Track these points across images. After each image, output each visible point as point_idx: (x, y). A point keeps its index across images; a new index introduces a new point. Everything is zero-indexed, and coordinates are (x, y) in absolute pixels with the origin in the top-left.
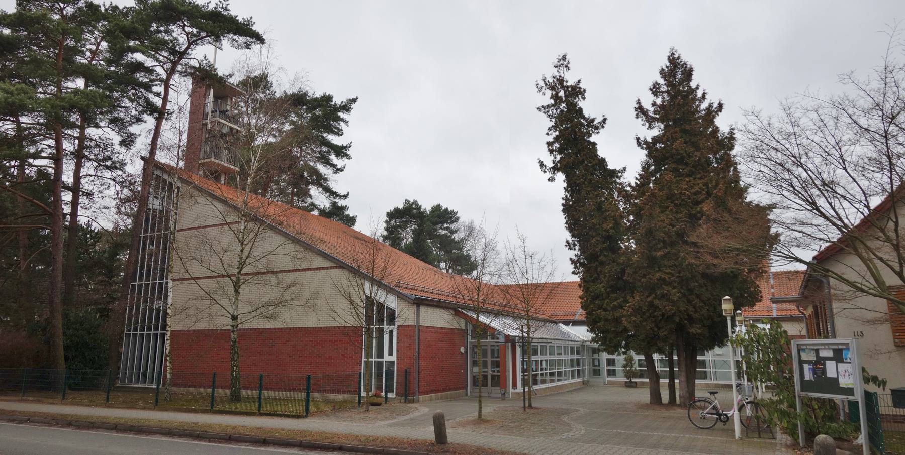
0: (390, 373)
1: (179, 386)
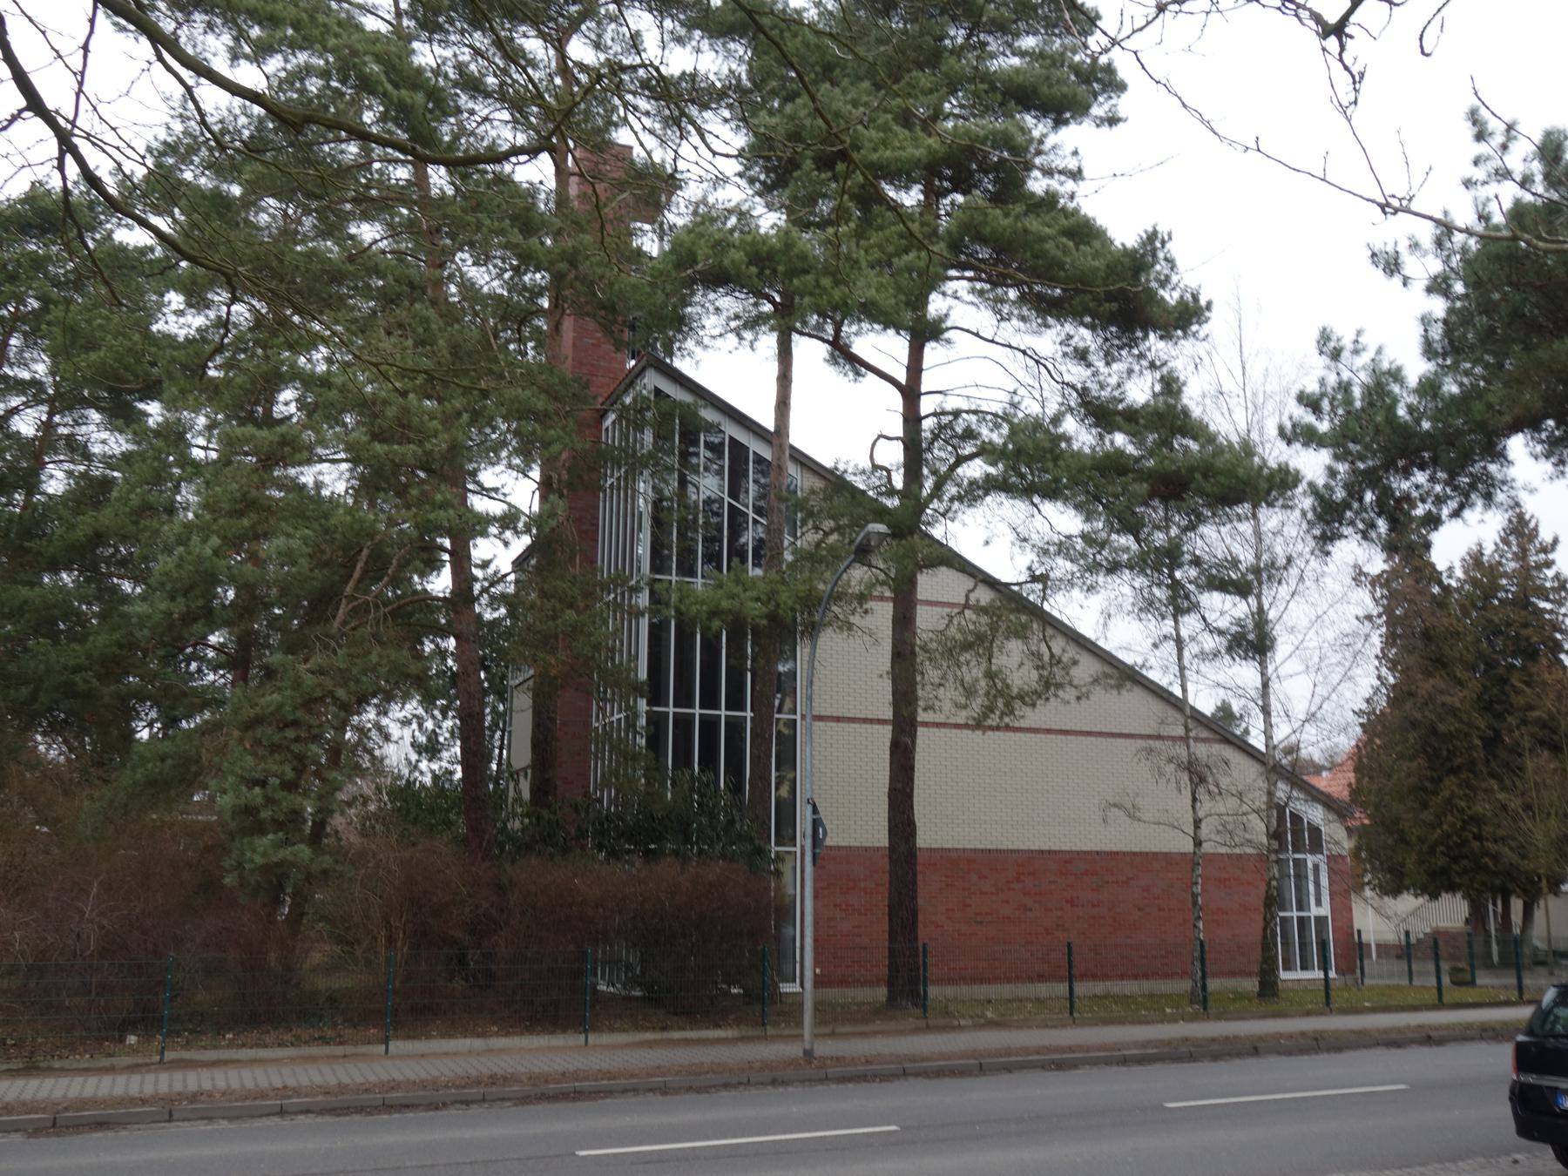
1: (844, 982)
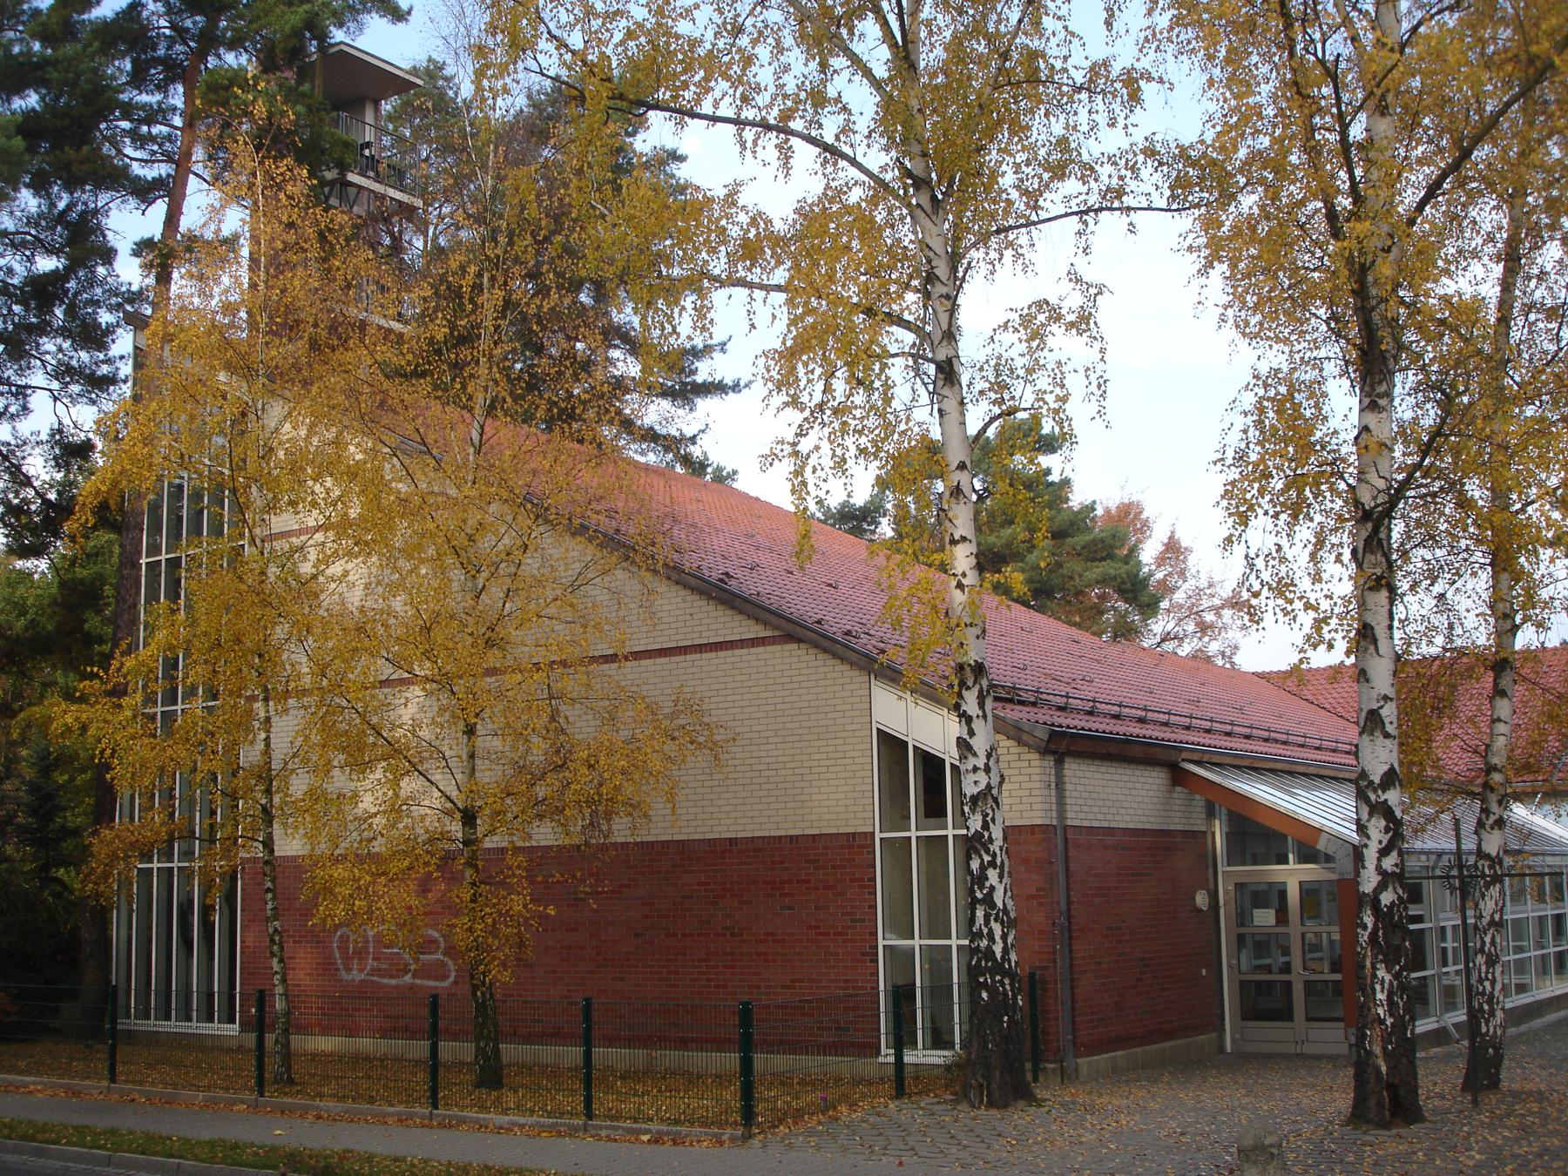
0: (939, 990)
